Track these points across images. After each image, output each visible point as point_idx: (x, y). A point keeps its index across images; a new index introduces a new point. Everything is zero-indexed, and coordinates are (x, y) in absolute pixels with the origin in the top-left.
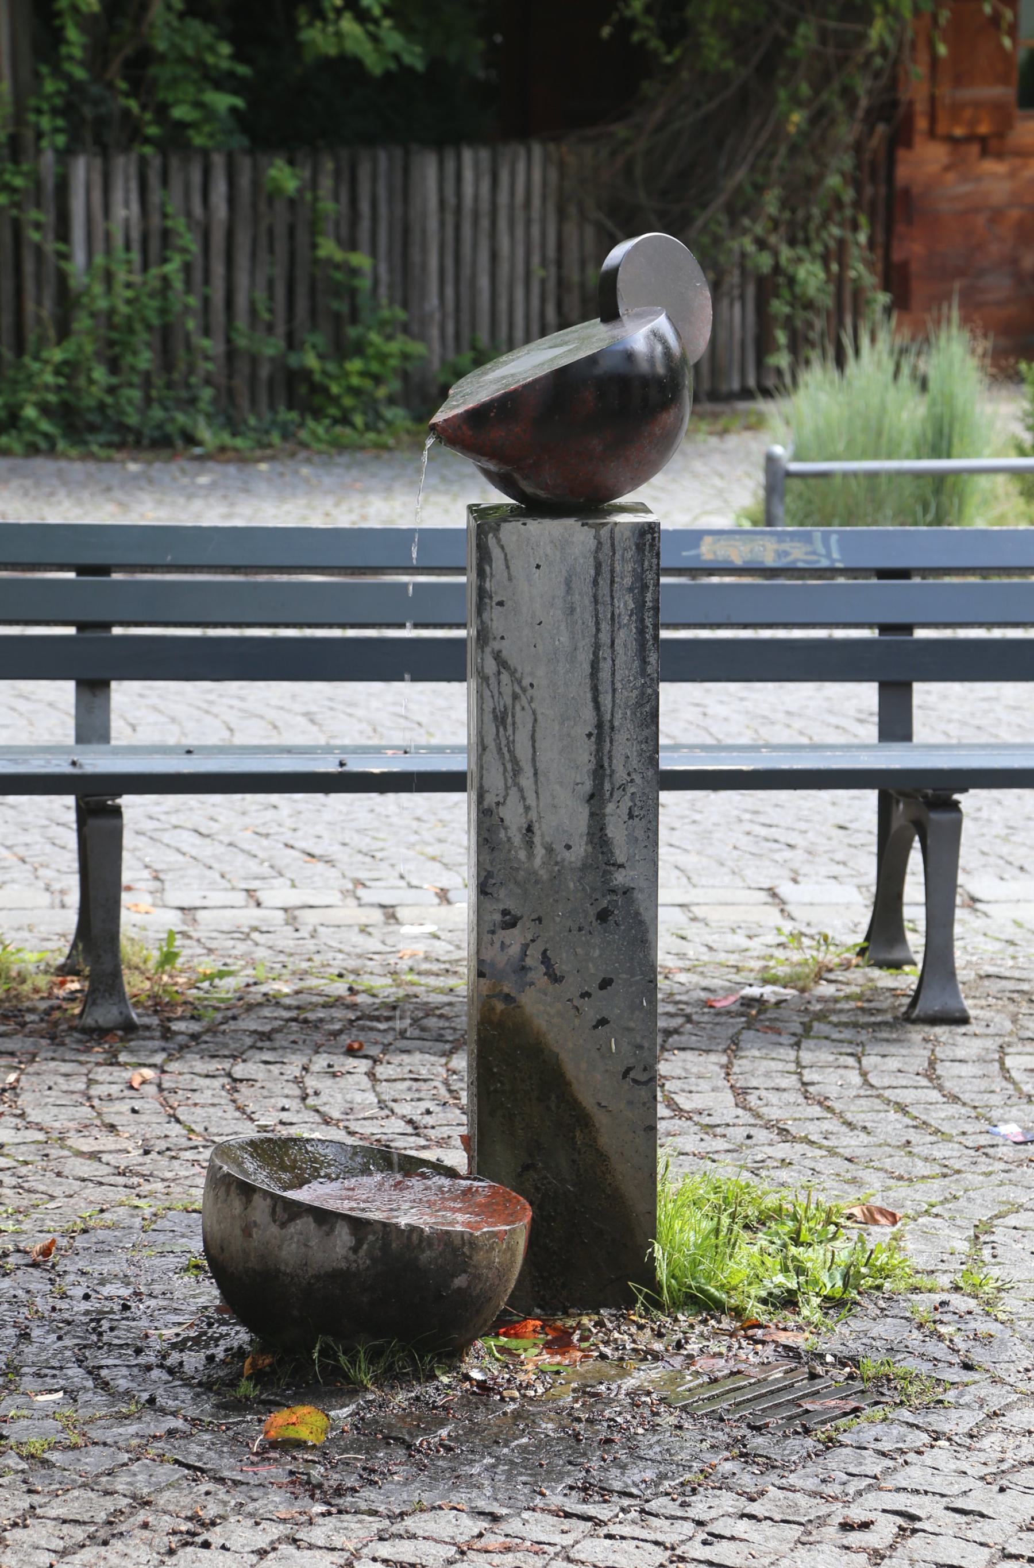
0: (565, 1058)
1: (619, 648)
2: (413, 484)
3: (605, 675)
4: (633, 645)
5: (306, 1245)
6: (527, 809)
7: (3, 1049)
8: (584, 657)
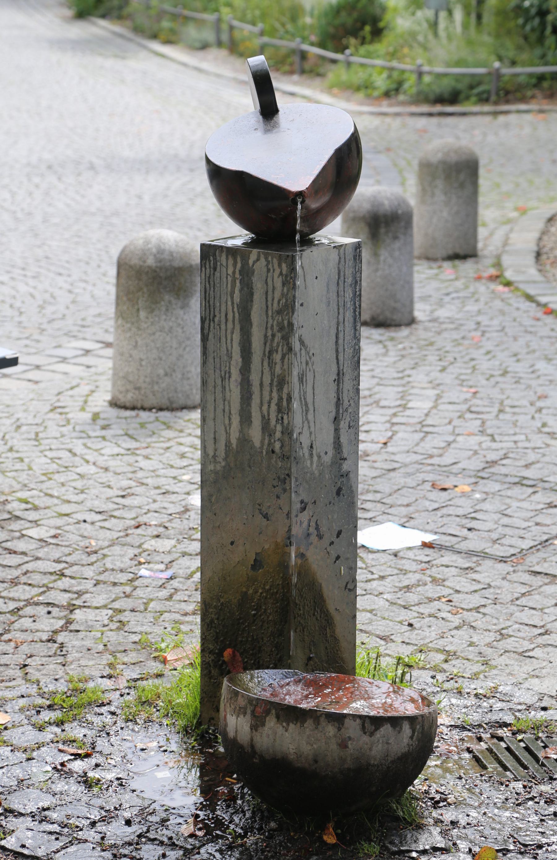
0: (323, 585)
1: (346, 323)
2: (160, 251)
3: (341, 341)
4: (352, 320)
5: (387, 743)
6: (311, 433)
7: (2, 663)
8: (333, 332)
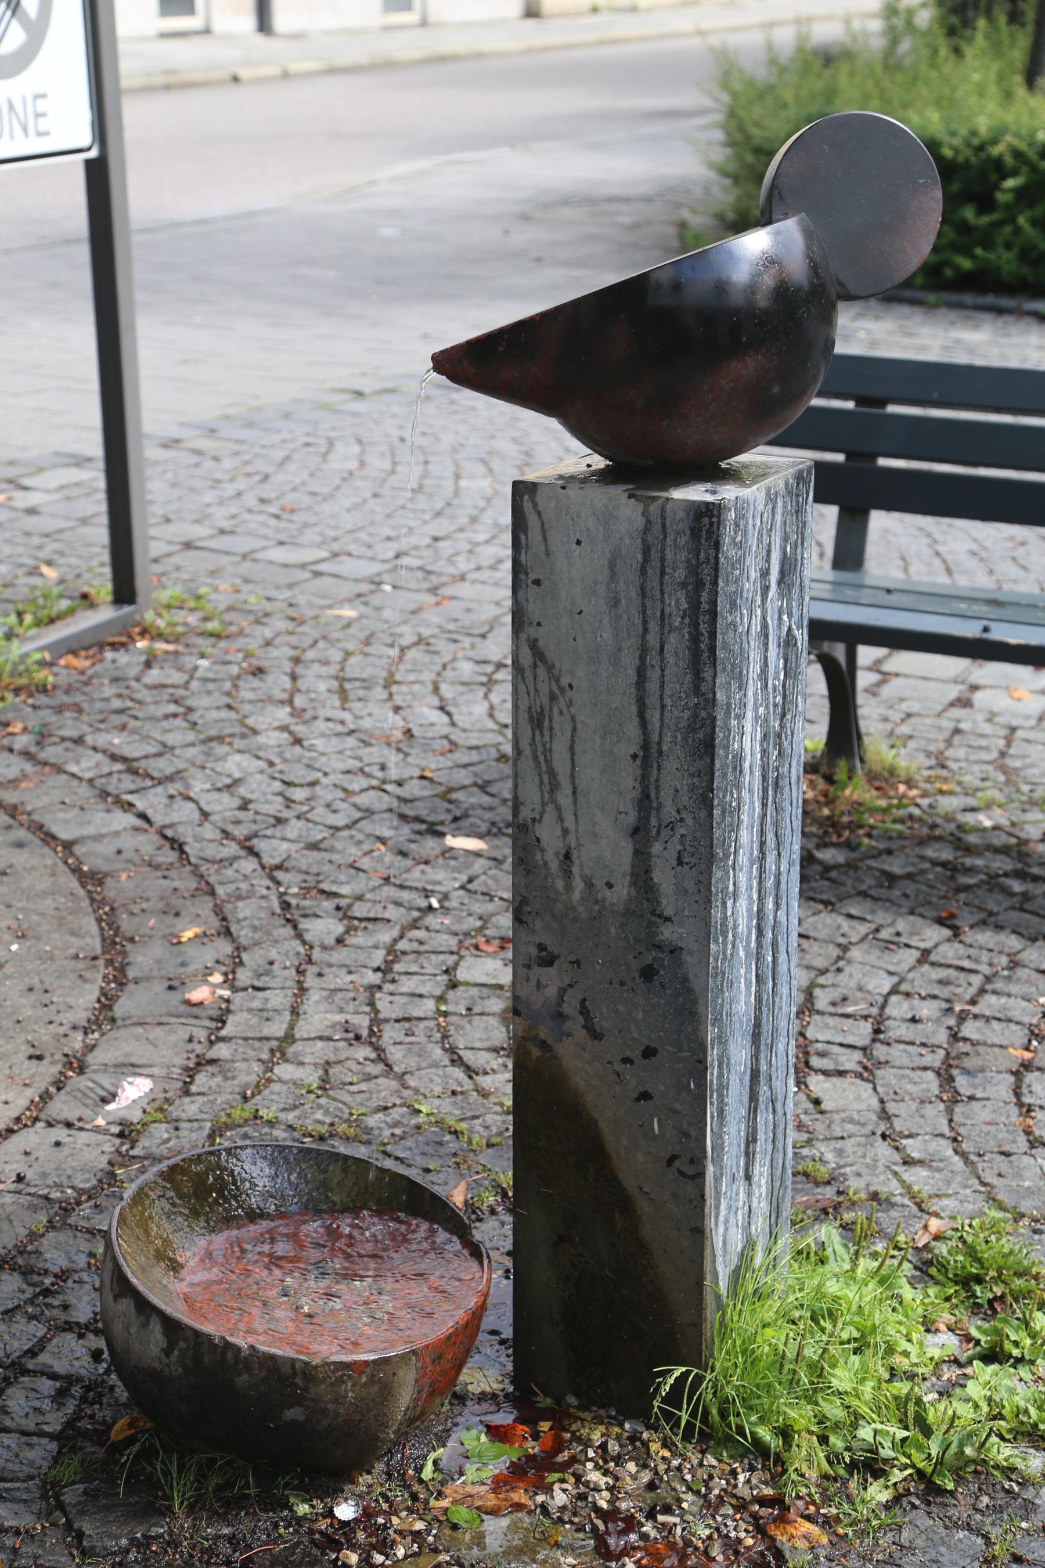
8: (629, 661)
